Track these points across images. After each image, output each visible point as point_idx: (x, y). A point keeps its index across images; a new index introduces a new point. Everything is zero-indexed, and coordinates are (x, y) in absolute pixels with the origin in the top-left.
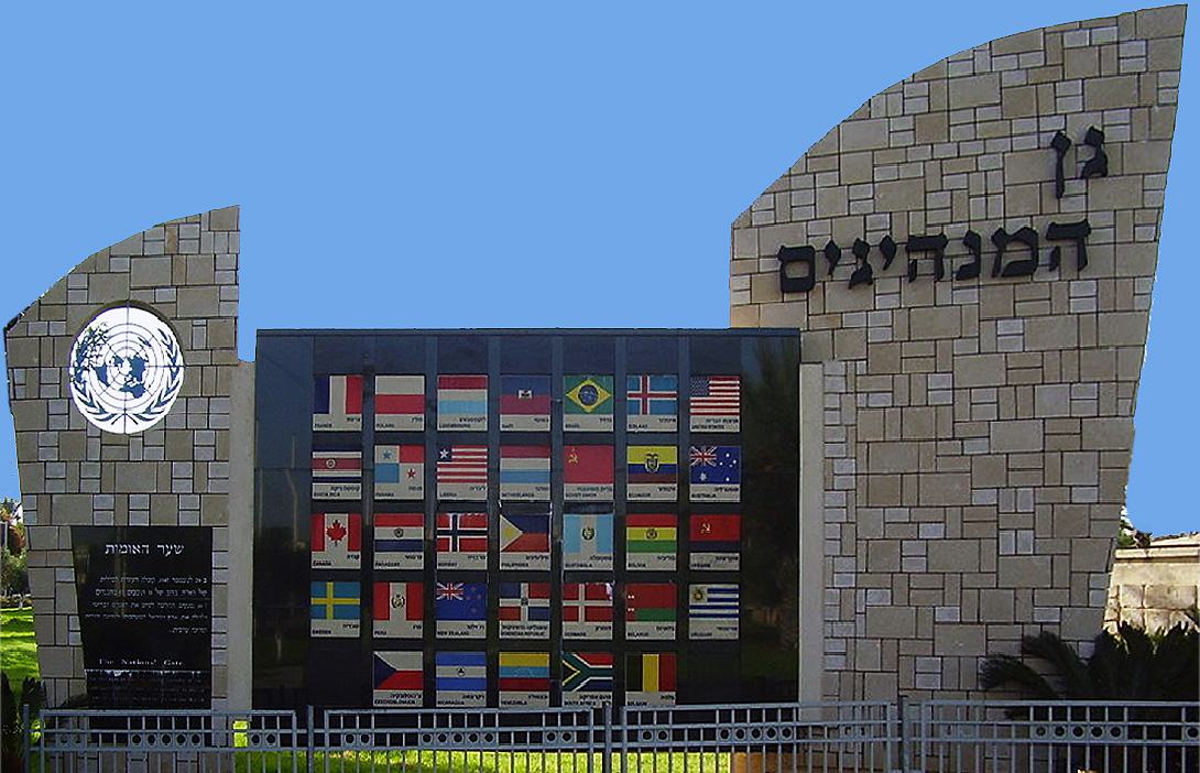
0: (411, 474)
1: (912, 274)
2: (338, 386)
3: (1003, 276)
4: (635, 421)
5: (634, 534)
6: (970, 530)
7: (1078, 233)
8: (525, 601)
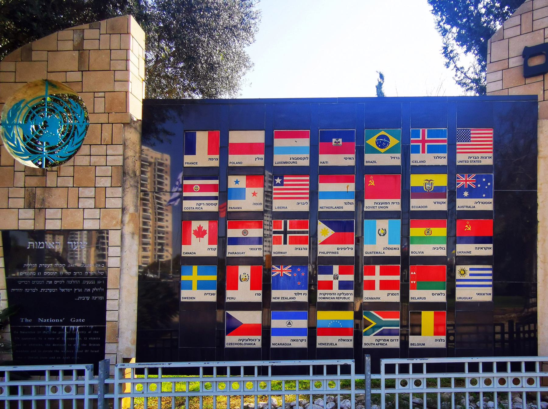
0: (254, 194)
2: (202, 139)
4: (416, 159)
8: (336, 276)
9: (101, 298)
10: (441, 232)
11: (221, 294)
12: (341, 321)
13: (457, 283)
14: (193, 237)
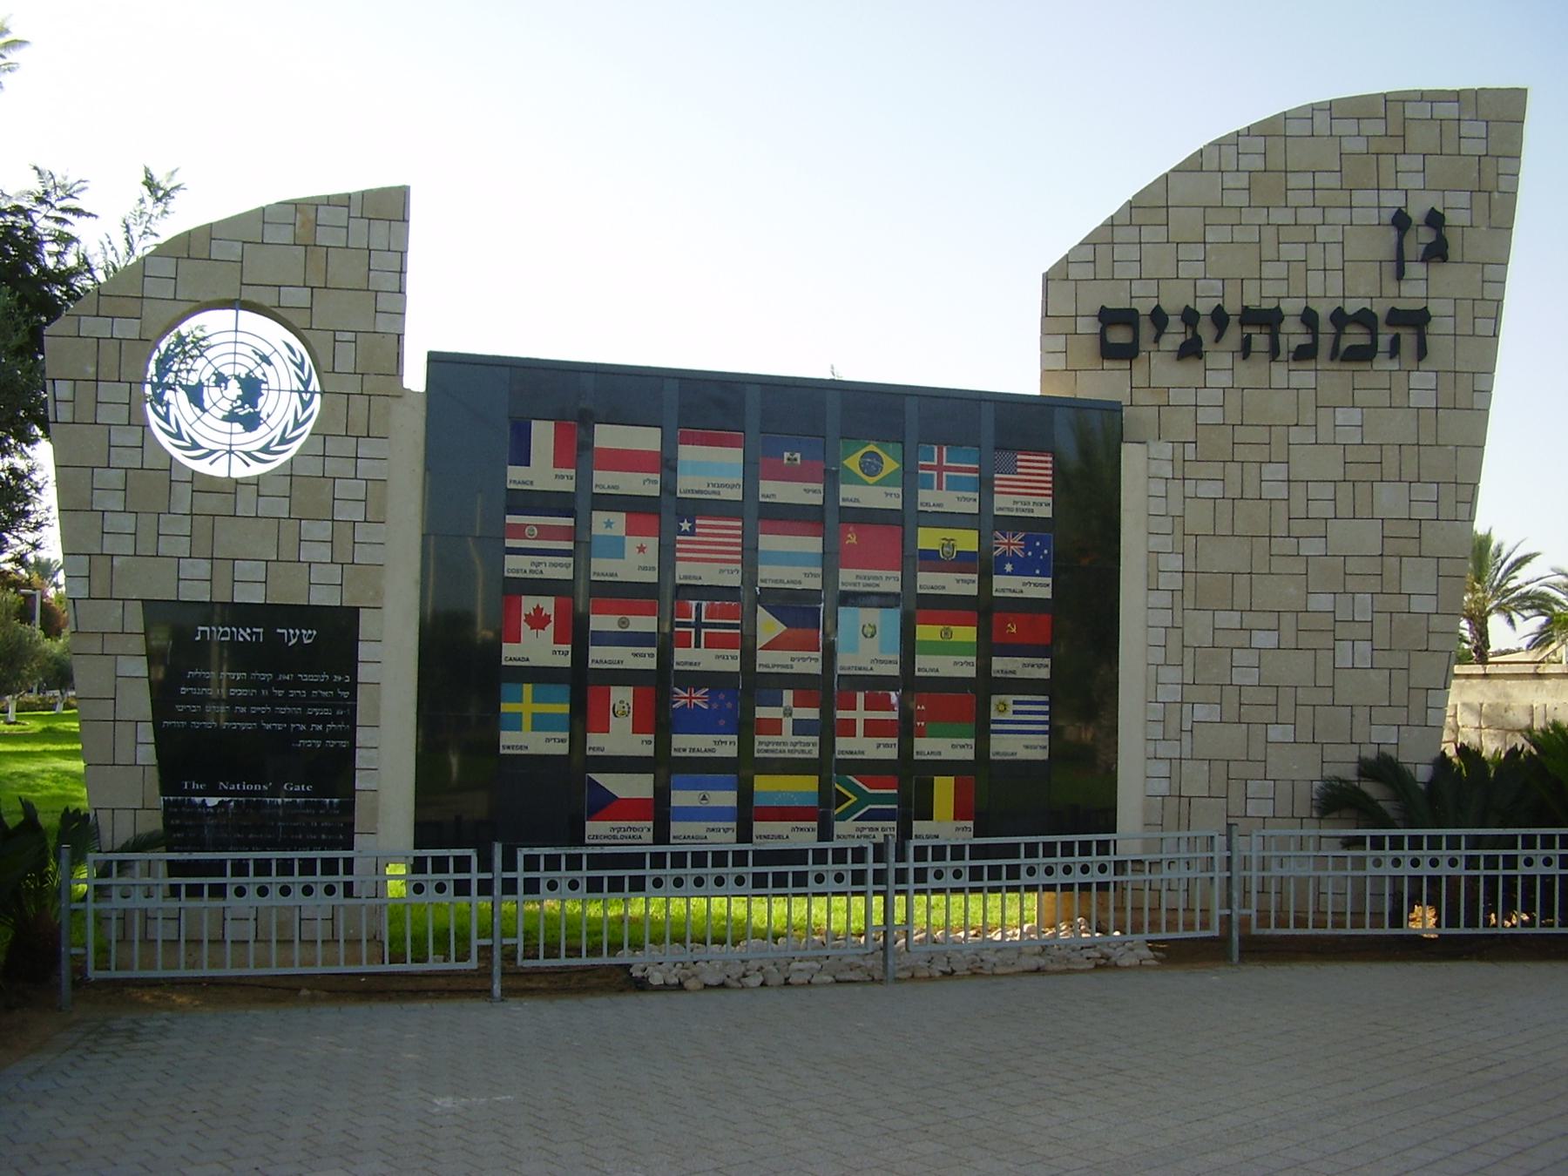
0: (641, 549)
2: (543, 434)
4: (928, 498)
7: (1418, 320)
8: (787, 711)
9: (344, 744)
10: (966, 634)
11: (577, 741)
12: (797, 794)
13: (993, 727)
14: (525, 627)
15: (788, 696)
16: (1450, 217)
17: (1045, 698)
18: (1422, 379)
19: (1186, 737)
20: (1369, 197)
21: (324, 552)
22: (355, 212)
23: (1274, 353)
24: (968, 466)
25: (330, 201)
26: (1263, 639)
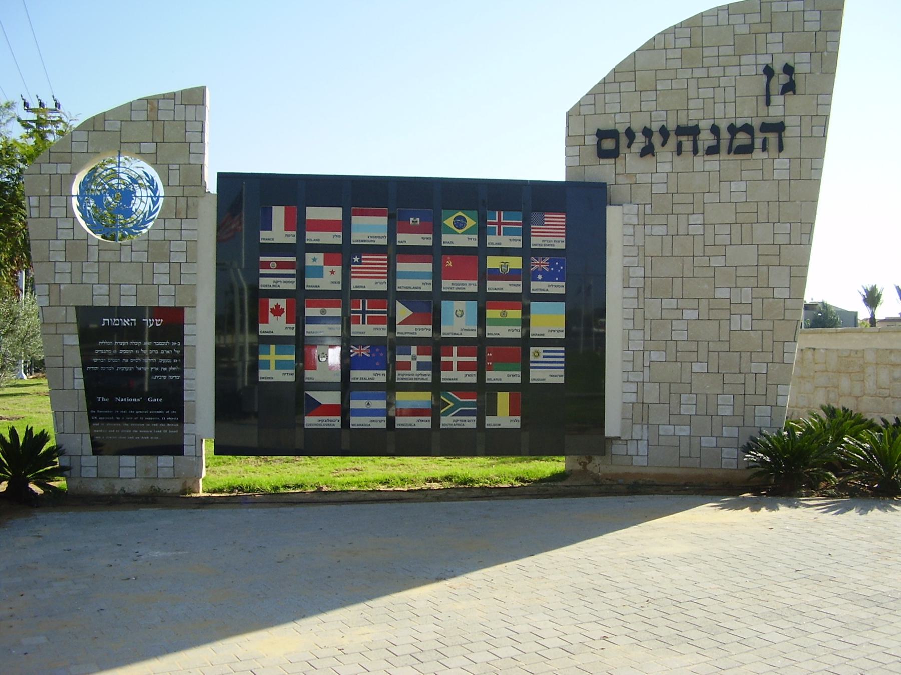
0: (332, 273)
1: (679, 151)
2: (279, 214)
3: (735, 153)
4: (492, 241)
5: (491, 314)
6: (714, 315)
7: (779, 128)
8: (414, 357)
9: (177, 377)
13: (531, 365)
14: (271, 315)
15: (414, 350)
16: (798, 69)
17: (563, 349)
18: (782, 163)
19: (646, 370)
20: (751, 59)
21: (165, 279)
22: (178, 102)
23: (695, 152)
24: (515, 221)
25: (164, 97)
26: (690, 315)
